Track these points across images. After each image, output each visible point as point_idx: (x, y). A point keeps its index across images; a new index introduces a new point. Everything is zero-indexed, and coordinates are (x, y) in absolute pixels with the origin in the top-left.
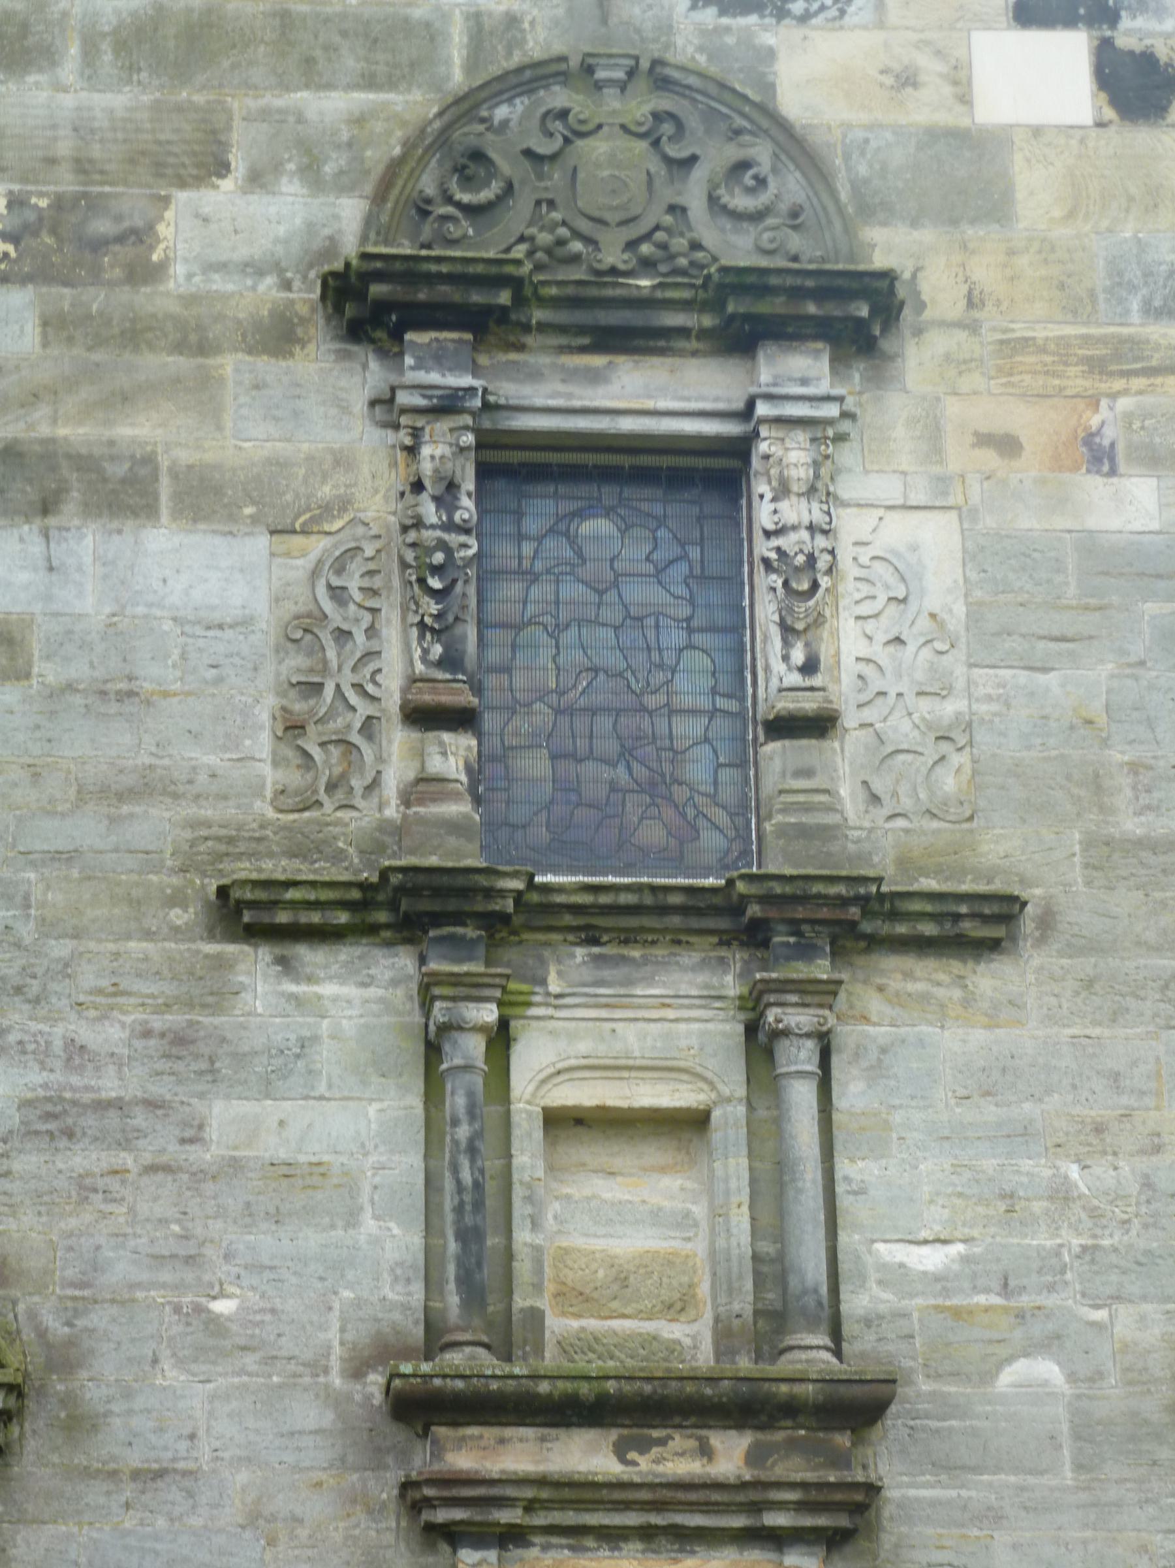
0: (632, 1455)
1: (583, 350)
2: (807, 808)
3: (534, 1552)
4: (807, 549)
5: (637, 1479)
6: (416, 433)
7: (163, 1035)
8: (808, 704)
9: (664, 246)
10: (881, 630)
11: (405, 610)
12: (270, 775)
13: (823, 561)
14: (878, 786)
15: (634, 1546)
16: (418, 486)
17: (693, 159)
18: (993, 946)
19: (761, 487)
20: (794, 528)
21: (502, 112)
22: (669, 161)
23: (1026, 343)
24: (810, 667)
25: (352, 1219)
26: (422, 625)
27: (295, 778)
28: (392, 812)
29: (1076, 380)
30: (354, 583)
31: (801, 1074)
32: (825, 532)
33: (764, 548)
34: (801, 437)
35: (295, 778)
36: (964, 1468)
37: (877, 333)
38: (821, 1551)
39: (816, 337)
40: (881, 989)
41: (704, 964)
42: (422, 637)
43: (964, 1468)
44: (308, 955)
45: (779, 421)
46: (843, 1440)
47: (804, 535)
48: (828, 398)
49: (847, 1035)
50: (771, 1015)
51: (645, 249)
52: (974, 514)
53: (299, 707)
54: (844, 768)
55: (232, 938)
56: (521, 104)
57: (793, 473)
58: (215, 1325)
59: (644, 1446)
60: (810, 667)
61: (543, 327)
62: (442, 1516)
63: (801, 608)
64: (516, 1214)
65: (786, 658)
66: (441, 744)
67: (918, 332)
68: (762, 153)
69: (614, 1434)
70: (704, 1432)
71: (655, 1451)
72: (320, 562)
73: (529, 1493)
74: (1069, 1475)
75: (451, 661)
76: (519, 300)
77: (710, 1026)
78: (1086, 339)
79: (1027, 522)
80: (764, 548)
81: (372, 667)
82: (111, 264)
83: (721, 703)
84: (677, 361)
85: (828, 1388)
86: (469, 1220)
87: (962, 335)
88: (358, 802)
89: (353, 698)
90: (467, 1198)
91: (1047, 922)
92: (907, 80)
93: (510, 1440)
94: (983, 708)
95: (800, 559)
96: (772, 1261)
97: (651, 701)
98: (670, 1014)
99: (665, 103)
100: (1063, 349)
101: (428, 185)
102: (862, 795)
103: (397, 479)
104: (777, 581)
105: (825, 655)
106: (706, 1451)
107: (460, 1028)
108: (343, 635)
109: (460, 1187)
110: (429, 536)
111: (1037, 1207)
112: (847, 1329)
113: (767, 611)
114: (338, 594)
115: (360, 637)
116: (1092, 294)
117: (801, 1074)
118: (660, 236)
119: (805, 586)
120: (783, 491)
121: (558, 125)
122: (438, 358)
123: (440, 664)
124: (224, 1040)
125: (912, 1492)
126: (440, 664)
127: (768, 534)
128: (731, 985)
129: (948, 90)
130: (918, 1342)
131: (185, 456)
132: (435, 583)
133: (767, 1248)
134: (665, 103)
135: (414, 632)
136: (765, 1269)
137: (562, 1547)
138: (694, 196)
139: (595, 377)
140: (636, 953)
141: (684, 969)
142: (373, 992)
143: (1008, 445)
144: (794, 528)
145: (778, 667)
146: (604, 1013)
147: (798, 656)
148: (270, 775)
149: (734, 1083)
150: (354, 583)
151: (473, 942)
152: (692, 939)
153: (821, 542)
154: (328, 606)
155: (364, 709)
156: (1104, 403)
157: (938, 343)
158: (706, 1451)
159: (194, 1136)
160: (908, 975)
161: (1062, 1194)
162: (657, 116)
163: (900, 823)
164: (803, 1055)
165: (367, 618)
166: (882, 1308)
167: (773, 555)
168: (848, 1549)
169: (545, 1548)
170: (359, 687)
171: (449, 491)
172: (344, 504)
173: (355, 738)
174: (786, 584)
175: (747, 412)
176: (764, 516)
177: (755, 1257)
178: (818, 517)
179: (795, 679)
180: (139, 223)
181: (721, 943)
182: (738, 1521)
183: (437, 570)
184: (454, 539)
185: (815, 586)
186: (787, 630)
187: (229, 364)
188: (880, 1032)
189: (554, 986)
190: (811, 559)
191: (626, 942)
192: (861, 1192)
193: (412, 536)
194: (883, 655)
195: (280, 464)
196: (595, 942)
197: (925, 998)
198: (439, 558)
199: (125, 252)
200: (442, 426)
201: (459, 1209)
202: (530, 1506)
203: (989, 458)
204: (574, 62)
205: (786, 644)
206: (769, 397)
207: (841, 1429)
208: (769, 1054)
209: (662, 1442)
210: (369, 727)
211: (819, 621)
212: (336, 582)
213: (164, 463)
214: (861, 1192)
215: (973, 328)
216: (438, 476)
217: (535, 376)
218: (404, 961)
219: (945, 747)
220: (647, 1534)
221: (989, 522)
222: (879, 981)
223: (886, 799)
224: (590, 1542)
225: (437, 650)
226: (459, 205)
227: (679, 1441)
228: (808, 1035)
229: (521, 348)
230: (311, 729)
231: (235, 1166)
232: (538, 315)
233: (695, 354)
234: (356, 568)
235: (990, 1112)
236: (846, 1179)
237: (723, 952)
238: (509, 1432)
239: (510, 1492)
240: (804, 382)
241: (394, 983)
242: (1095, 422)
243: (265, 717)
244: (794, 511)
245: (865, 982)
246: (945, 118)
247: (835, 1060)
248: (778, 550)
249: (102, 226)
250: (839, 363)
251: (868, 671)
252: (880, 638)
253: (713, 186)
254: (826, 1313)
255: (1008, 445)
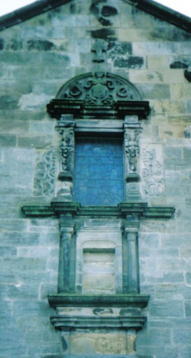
0: (97, 313)
1: (94, 118)
2: (164, 212)
3: (76, 333)
4: (134, 149)
5: (97, 317)
6: (63, 131)
7: (10, 235)
8: (134, 176)
9: (108, 102)
10: (148, 164)
11: (59, 161)
12: (33, 189)
13: (137, 151)
14: (147, 190)
15: (97, 331)
16: (63, 140)
17: (114, 88)
18: (168, 218)
19: (126, 140)
20: (131, 146)
21: (80, 82)
22: (109, 88)
23: (173, 117)
24: (135, 170)
25: (44, 268)
26: (63, 163)
27: (37, 190)
28: (56, 196)
29: (182, 123)
30: (51, 157)
31: (132, 240)
32: (138, 146)
33: (126, 149)
34: (133, 130)
35: (37, 190)
36: (165, 316)
37: (146, 114)
38: (135, 332)
39: (135, 114)
40: (148, 226)
41: (114, 222)
42: (62, 165)
43: (165, 316)
44: (40, 221)
45: (129, 128)
46: (139, 309)
47: (133, 147)
48: (137, 124)
49: (141, 233)
50: (127, 229)
51: (105, 102)
52: (164, 144)
53: (39, 178)
54: (141, 187)
55: (25, 218)
56: (84, 80)
57: (131, 137)
58: (15, 289)
59: (99, 311)
60: (135, 170)
61: (87, 114)
62: (58, 325)
63: (132, 159)
64: (77, 268)
65: (130, 168)
66: (66, 184)
67: (154, 115)
68: (126, 87)
69: (93, 308)
70: (111, 308)
71: (101, 312)
72: (45, 153)
73: (75, 320)
74: (185, 316)
75: (68, 169)
76: (82, 109)
77: (115, 233)
78: (183, 116)
79: (174, 146)
80: (126, 149)
81: (53, 171)
82: (10, 106)
83: (119, 179)
84: (110, 120)
85: (15, 22)
86: (66, 268)
87: (162, 116)
88: (49, 194)
89: (49, 176)
90: (66, 264)
91: (179, 214)
92: (151, 77)
93: (80, 7)
94: (166, 177)
95: (133, 151)
96: (126, 277)
97: (106, 178)
98: (107, 231)
99: (109, 80)
100: (180, 118)
101: (67, 92)
102: (144, 192)
103: (59, 139)
104: (128, 155)
105: (137, 167)
106: (111, 312)
107: (66, 232)
108: (48, 166)
109: (65, 262)
110: (64, 148)
111: (178, 265)
112: (141, 289)
113: (127, 161)
114: (48, 159)
115: (51, 166)
116: (185, 109)
117: (132, 240)
118: (108, 100)
119: (133, 155)
120: (130, 140)
121: (90, 83)
122: (67, 118)
123: (66, 170)
124: (21, 236)
125: (155, 320)
126: (66, 170)
127: (127, 147)
128: (119, 225)
129: (158, 79)
130: (155, 291)
131: (21, 136)
132: (65, 155)
133: (126, 274)
134: (109, 80)
135: (61, 165)
136: (126, 278)
137: (82, 331)
138: (114, 94)
139: (96, 123)
140: (101, 220)
141: (110, 223)
142: (50, 227)
143: (170, 133)
144: (131, 146)
145: (129, 170)
146: (95, 231)
147: (133, 168)
148: (33, 189)
149: (119, 243)
150: (51, 157)
151: (70, 217)
152: (112, 217)
153: (136, 148)
154: (46, 161)
155: (51, 178)
156: (187, 127)
157: (158, 117)
158: (111, 312)
159: (15, 252)
160: (153, 224)
161: (183, 263)
162: (108, 82)
163: (152, 197)
164: (133, 236)
165: (53, 163)
166: (148, 285)
167: (128, 150)
168: (141, 332)
169: (79, 331)
170: (51, 175)
171: (68, 141)
172: (50, 144)
173: (49, 183)
174: (130, 155)
175: (123, 128)
176: (126, 144)
177: (123, 276)
178: (136, 143)
179: (132, 172)
180: (15, 99)
181: (118, 218)
182: (119, 326)
183: (65, 153)
184: (68, 148)
185: (135, 155)
186: (131, 163)
187: (30, 122)
188: (148, 234)
189: (85, 226)
190: (135, 151)
191: (99, 218)
192: (144, 263)
193: (61, 147)
194: (148, 168)
195: (39, 138)
196: (93, 218)
197: (157, 227)
198: (66, 151)
199: (13, 104)
200: (68, 129)
201: (64, 266)
202: (76, 322)
203: (167, 135)
204: (93, 74)
205: (130, 166)
206: (127, 124)
207: (139, 307)
208: (126, 237)
209: (103, 310)
210: (52, 181)
211: (136, 162)
212: (48, 156)
213: (17, 137)
214: (144, 263)
215: (164, 114)
216: (66, 137)
217: (85, 123)
218: (56, 222)
219: (160, 184)
220: (100, 328)
221: (167, 146)
222: (147, 224)
223: (149, 192)
224: (88, 330)
225: (65, 167)
226: (72, 95)
227: (106, 309)
228: (133, 233)
229: (82, 118)
230: (41, 181)
231: (21, 259)
232: (85, 112)
233: (114, 119)
234: (51, 154)
235: (168, 248)
236: (141, 261)
237: (118, 219)
238: (73, 308)
239: (71, 320)
240: (133, 121)
241: (55, 226)
242: (186, 130)
243: (33, 179)
244: (131, 143)
245: (145, 225)
246: (159, 82)
247: (139, 239)
248: (129, 149)
249: (9, 100)
250: (140, 119)
251: (146, 171)
252: (148, 165)
253: (117, 92)
254: (136, 286)
255: (170, 133)
